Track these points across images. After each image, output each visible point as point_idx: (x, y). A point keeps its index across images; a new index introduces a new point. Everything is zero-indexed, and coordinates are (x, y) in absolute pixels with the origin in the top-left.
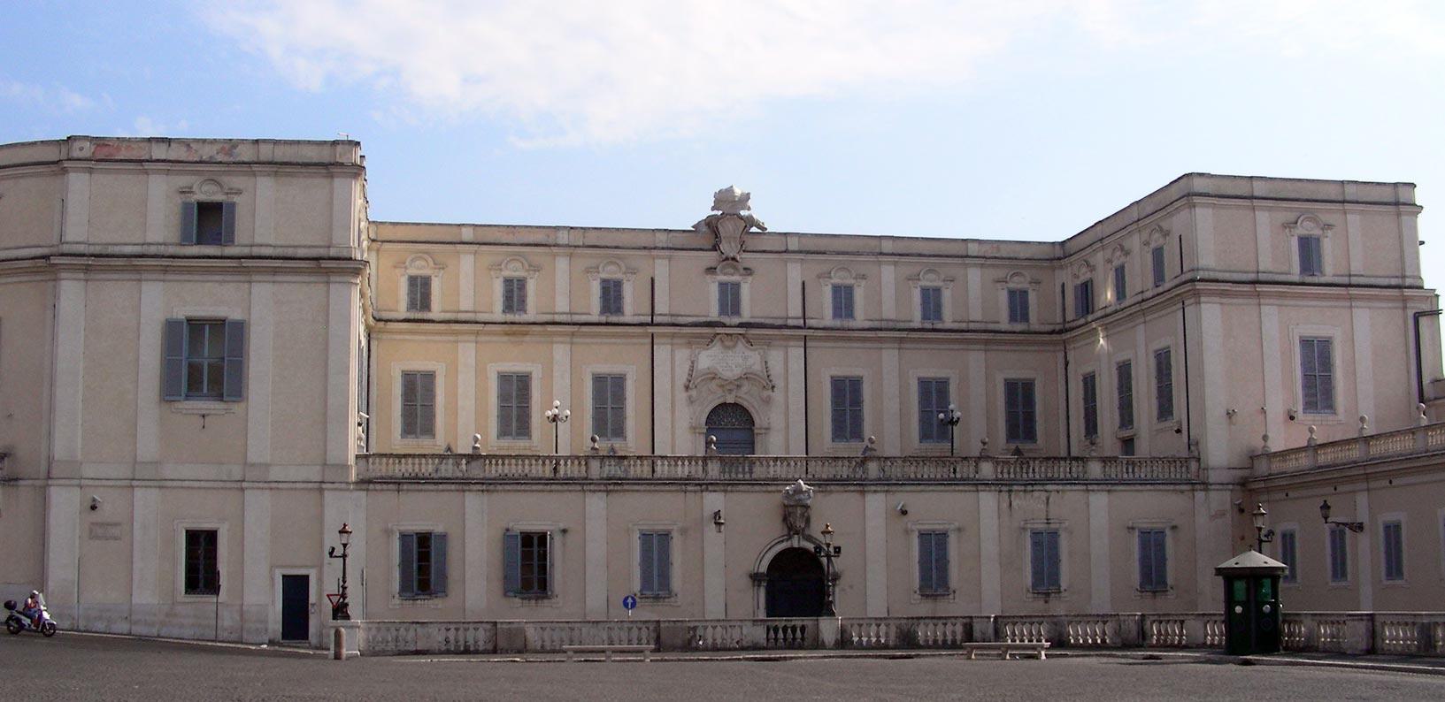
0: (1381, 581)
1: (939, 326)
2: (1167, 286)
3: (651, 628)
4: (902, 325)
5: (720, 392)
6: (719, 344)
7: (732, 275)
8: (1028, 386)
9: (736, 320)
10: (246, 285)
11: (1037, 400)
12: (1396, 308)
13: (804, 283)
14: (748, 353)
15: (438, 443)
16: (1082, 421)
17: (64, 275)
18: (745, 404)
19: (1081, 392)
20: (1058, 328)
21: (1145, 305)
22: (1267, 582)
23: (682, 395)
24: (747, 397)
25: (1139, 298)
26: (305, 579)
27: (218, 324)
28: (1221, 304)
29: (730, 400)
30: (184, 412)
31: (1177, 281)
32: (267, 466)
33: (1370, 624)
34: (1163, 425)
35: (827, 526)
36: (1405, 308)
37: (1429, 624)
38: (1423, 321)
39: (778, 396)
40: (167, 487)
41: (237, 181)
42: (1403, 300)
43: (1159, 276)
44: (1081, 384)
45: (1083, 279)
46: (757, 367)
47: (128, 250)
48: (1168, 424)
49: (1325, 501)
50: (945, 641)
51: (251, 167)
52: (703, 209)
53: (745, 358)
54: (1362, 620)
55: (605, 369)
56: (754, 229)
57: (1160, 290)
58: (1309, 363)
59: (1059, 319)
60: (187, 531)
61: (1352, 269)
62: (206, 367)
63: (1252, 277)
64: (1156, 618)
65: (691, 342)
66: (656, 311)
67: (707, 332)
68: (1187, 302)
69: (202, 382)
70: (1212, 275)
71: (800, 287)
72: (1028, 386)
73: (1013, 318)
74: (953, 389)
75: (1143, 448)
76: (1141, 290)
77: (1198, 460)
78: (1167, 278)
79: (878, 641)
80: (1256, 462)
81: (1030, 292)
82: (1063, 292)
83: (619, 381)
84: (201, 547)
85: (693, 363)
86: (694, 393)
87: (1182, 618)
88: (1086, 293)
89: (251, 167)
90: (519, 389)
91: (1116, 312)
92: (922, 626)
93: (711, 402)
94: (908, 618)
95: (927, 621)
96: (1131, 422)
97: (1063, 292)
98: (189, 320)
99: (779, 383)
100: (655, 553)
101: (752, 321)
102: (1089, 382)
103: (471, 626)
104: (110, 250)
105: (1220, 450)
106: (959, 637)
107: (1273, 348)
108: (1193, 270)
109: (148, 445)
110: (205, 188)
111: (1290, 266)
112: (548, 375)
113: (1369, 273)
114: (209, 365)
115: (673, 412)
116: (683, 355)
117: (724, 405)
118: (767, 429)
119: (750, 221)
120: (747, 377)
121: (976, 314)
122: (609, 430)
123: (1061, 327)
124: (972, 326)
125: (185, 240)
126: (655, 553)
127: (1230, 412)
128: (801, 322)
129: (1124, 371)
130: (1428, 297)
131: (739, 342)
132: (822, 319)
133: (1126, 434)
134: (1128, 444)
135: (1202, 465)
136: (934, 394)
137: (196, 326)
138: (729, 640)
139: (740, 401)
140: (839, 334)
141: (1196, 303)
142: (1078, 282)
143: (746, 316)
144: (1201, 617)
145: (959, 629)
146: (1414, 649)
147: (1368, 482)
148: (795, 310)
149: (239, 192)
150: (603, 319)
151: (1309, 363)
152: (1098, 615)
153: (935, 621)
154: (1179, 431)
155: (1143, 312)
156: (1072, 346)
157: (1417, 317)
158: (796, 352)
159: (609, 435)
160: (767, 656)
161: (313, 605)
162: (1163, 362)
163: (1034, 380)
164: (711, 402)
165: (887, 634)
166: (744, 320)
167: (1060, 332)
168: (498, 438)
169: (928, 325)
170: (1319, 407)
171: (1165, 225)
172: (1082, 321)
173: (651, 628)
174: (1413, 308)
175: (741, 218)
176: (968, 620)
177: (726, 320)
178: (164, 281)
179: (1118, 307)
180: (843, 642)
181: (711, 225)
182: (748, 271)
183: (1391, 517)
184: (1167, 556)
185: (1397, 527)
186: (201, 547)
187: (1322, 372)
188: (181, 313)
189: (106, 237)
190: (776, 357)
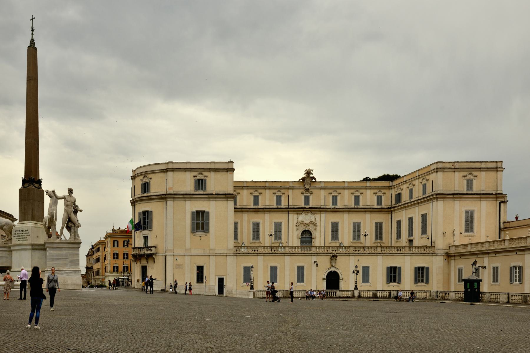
0: (491, 283)
1: (359, 207)
2: (427, 195)
3: (317, 292)
4: (349, 207)
6: (304, 213)
7: (308, 194)
8: (381, 224)
9: (308, 207)
10: (209, 202)
11: (383, 228)
12: (494, 201)
13: (325, 195)
14: (311, 216)
15: (239, 242)
16: (396, 234)
17: (168, 200)
18: (310, 230)
19: (396, 227)
20: (389, 207)
21: (420, 201)
22: (476, 284)
23: (295, 228)
24: (311, 228)
25: (417, 199)
26: (223, 279)
27: (203, 212)
28: (443, 201)
29: (307, 229)
30: (196, 235)
31: (430, 194)
32: (215, 249)
33: (508, 295)
34: (422, 236)
37: (527, 296)
38: (502, 204)
39: (318, 228)
41: (205, 174)
42: (496, 198)
43: (424, 192)
44: (396, 224)
45: (398, 192)
46: (313, 220)
47: (182, 193)
48: (425, 236)
49: (476, 260)
50: (384, 297)
51: (209, 170)
52: (302, 175)
53: (310, 217)
54: (506, 294)
55: (276, 221)
56: (313, 180)
57: (425, 196)
58: (467, 218)
59: (390, 204)
60: (197, 267)
61: (482, 189)
62: (200, 223)
64: (441, 292)
65: (297, 213)
66: (289, 205)
67: (300, 210)
68: (433, 201)
69: (199, 228)
70: (442, 192)
72: (381, 224)
73: (378, 204)
74: (362, 225)
75: (416, 243)
76: (418, 196)
78: (427, 193)
79: (368, 296)
80: (451, 248)
81: (383, 196)
82: (391, 196)
83: (280, 224)
84: (200, 270)
85: (298, 218)
86: (298, 227)
87: (448, 292)
88: (399, 197)
89: (209, 170)
90: (257, 227)
91: (409, 203)
92: (378, 292)
93: (302, 229)
94: (375, 290)
95: (380, 291)
96: (412, 235)
97: (391, 196)
98: (197, 211)
99: (318, 224)
100: (495, 276)
101: (312, 206)
102: (399, 223)
103: (260, 291)
104: (178, 193)
105: (441, 245)
106: (387, 296)
108: (436, 191)
109: (188, 245)
110: (199, 176)
112: (242, 221)
114: (199, 220)
115: (293, 233)
116: (295, 216)
118: (315, 237)
119: (313, 178)
120: (311, 223)
121: (368, 204)
122: (278, 238)
123: (390, 206)
124: (367, 207)
125: (196, 190)
126: (495, 276)
127: (445, 233)
128: (324, 207)
129: (411, 220)
130: (504, 197)
131: (309, 213)
133: (411, 238)
134: (411, 241)
136: (357, 226)
137: (198, 212)
138: (403, 296)
139: (309, 229)
140: (335, 211)
141: (436, 201)
142: (397, 193)
143: (311, 205)
144: (454, 292)
145: (388, 294)
146: (520, 302)
147: (488, 254)
148: (323, 204)
149: (207, 177)
150: (277, 207)
151: (467, 218)
152: (425, 291)
153: (382, 291)
154: (428, 238)
155: (419, 203)
156: (394, 212)
159: (278, 239)
160: (344, 299)
161: (225, 285)
162: (424, 217)
164: (302, 229)
165: (371, 294)
166: (310, 206)
167: (390, 208)
168: (252, 240)
169: (356, 207)
170: (469, 231)
171: (402, 188)
172: (397, 205)
173: (317, 292)
175: (311, 177)
176: (390, 291)
177: (306, 207)
178: (191, 201)
179: (410, 201)
180: (359, 296)
181: (303, 179)
182: (312, 193)
183: (495, 265)
184: (370, 274)
185: (497, 268)
186: (200, 270)
187: (471, 220)
188: (194, 210)
190: (318, 216)
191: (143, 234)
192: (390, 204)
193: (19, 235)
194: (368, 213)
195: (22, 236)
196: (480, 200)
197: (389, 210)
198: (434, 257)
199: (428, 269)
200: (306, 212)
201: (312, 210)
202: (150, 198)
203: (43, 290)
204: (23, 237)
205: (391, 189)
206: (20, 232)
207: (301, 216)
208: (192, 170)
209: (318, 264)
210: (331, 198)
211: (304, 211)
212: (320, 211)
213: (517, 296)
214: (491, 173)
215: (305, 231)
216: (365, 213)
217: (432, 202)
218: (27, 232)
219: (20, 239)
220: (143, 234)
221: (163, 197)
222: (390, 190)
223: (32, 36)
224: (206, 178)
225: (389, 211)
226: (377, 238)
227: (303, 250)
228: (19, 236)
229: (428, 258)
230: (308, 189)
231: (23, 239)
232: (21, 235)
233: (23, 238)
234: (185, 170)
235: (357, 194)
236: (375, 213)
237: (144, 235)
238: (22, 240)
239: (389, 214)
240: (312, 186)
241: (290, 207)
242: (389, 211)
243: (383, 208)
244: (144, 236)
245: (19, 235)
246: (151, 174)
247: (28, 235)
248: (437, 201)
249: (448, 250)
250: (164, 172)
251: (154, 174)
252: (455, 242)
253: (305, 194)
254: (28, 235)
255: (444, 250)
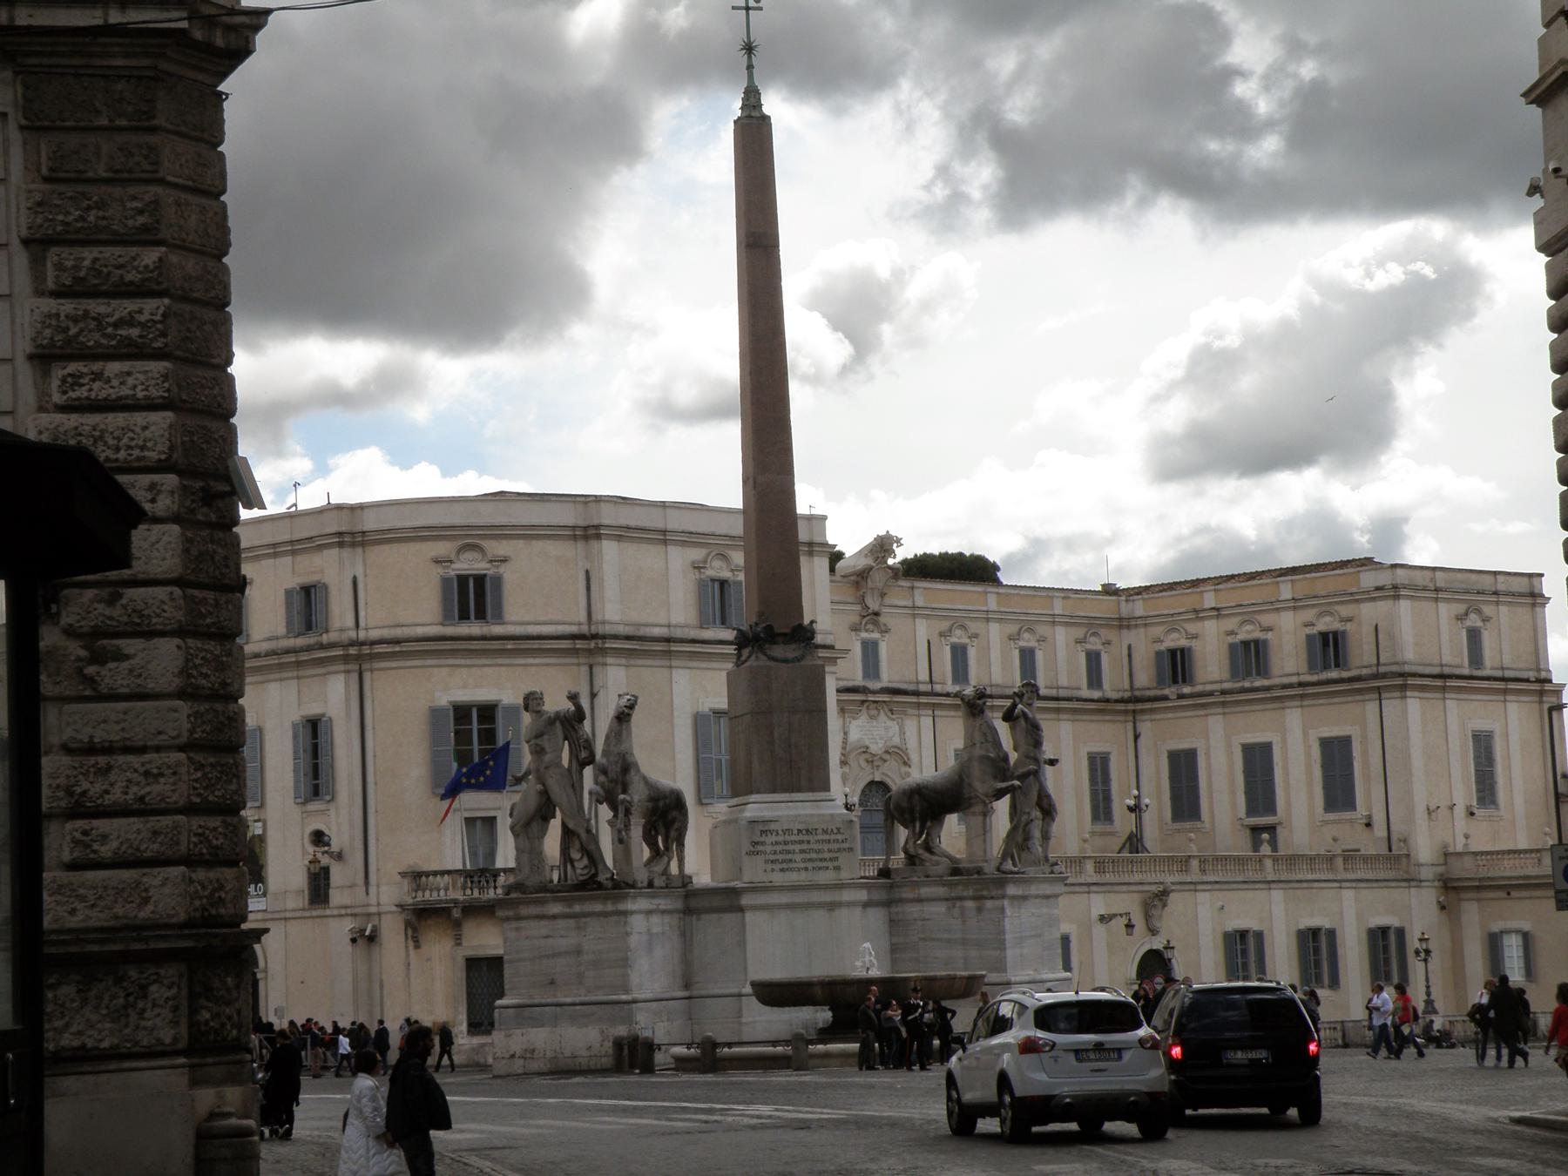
5: (868, 768)
14: (889, 723)
17: (610, 660)
35: (1423, 934)
36: (1541, 702)
38: (1555, 714)
40: (840, 905)
53: (887, 729)
63: (1436, 670)
71: (926, 645)
77: (1408, 856)
81: (1103, 654)
82: (1130, 656)
85: (845, 733)
96: (1271, 808)
97: (1130, 656)
99: (914, 757)
104: (643, 632)
107: (1455, 743)
111: (1462, 660)
113: (1515, 666)
117: (872, 783)
129: (1258, 762)
132: (944, 684)
135: (1412, 861)
141: (1402, 698)
148: (924, 676)
157: (1551, 710)
158: (927, 722)
163: (1109, 753)
174: (1547, 702)
175: (890, 567)
182: (885, 631)
189: (635, 617)
190: (910, 725)
191: (465, 810)
192: (1127, 686)
193: (790, 847)
194: (1065, 716)
195: (803, 851)
196: (1502, 698)
197: (1131, 707)
198: (1412, 890)
199: (1259, 936)
200: (872, 706)
201: (895, 699)
202: (509, 647)
203: (448, 1098)
204: (808, 856)
205: (1128, 627)
206: (797, 838)
207: (855, 723)
208: (689, 539)
209: (1133, 926)
210: (947, 650)
211: (867, 704)
212: (919, 706)
213: (1330, 1028)
214: (1519, 610)
215: (872, 784)
216: (1054, 716)
217: (1380, 700)
218: (833, 837)
219: (791, 865)
220: (465, 810)
221: (580, 644)
222: (1125, 632)
223: (750, 77)
224: (1269, 636)
225: (1126, 712)
226: (1096, 817)
227: (1155, 871)
228: (789, 852)
229: (1398, 895)
230: (877, 614)
231: (810, 865)
232: (797, 847)
233: (804, 861)
234: (663, 537)
235: (1028, 641)
236: (1085, 717)
237: (467, 815)
238: (806, 869)
239: (1126, 721)
240: (887, 601)
241: (938, 688)
242: (1126, 712)
243: (1107, 701)
244: (466, 819)
245: (790, 847)
246: (504, 542)
247: (839, 850)
248: (1406, 697)
249: (1443, 867)
250: (575, 538)
251: (520, 543)
252: (1469, 841)
253: (864, 635)
254: (839, 850)
255: (1435, 868)
